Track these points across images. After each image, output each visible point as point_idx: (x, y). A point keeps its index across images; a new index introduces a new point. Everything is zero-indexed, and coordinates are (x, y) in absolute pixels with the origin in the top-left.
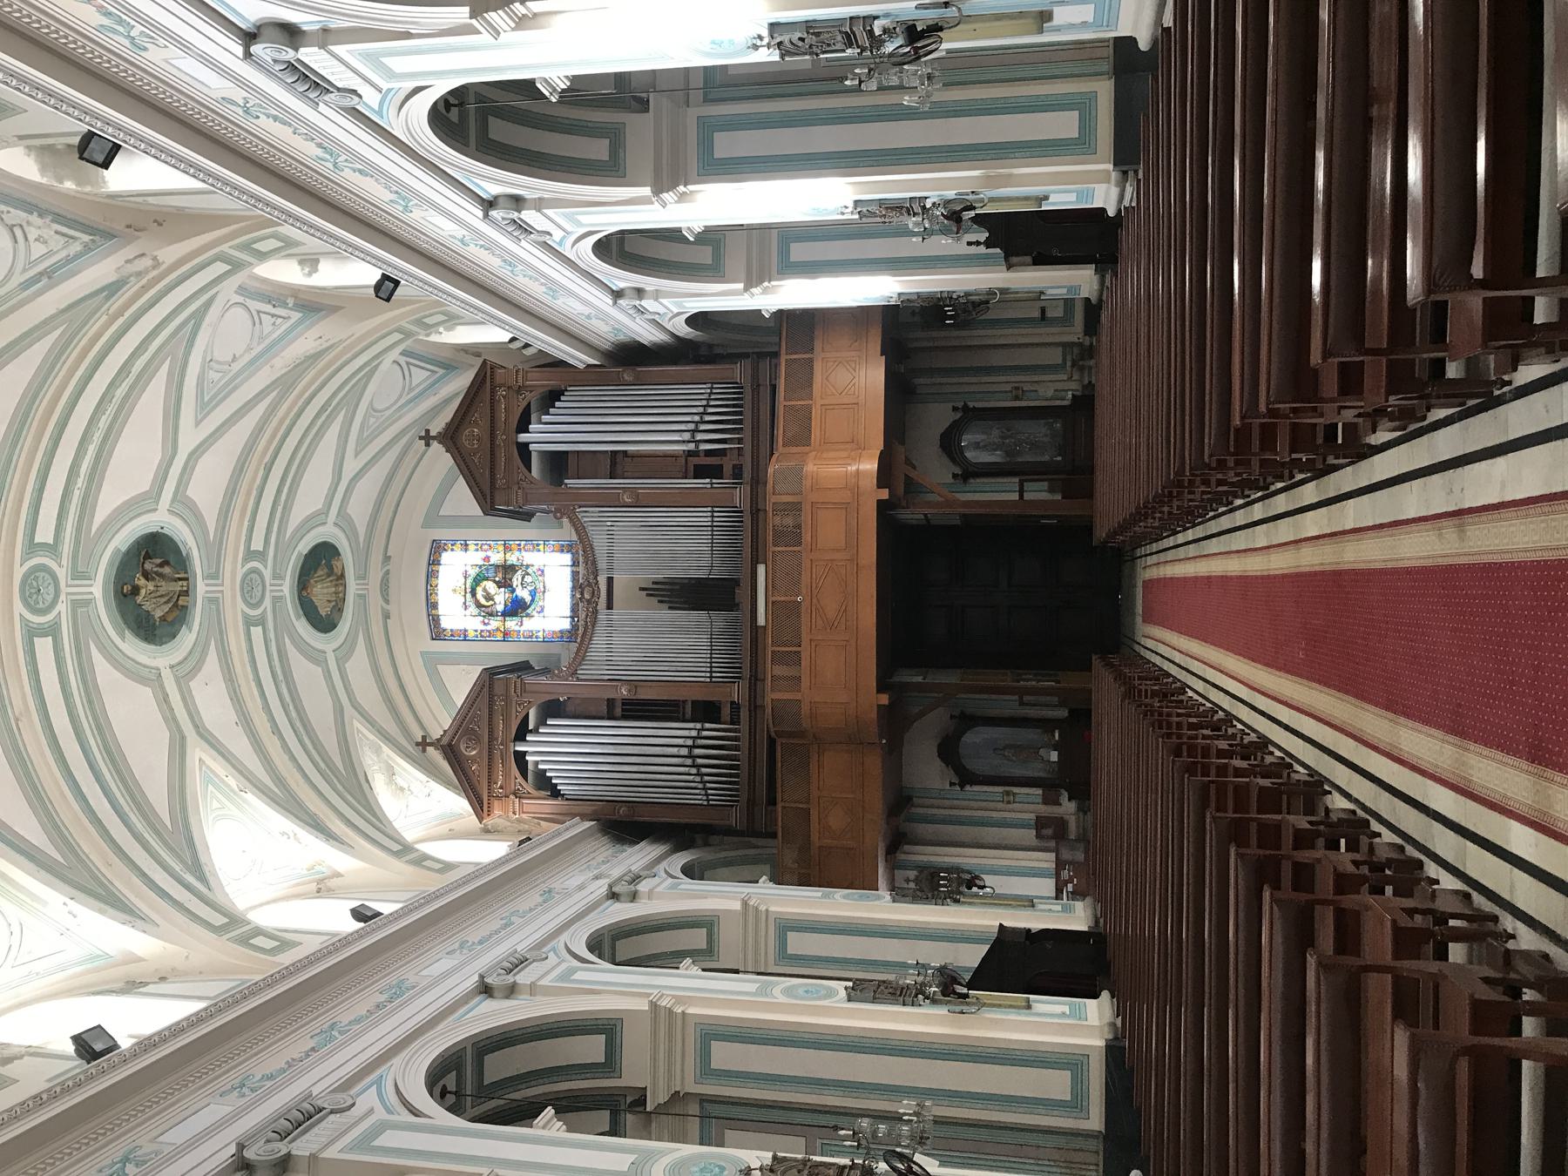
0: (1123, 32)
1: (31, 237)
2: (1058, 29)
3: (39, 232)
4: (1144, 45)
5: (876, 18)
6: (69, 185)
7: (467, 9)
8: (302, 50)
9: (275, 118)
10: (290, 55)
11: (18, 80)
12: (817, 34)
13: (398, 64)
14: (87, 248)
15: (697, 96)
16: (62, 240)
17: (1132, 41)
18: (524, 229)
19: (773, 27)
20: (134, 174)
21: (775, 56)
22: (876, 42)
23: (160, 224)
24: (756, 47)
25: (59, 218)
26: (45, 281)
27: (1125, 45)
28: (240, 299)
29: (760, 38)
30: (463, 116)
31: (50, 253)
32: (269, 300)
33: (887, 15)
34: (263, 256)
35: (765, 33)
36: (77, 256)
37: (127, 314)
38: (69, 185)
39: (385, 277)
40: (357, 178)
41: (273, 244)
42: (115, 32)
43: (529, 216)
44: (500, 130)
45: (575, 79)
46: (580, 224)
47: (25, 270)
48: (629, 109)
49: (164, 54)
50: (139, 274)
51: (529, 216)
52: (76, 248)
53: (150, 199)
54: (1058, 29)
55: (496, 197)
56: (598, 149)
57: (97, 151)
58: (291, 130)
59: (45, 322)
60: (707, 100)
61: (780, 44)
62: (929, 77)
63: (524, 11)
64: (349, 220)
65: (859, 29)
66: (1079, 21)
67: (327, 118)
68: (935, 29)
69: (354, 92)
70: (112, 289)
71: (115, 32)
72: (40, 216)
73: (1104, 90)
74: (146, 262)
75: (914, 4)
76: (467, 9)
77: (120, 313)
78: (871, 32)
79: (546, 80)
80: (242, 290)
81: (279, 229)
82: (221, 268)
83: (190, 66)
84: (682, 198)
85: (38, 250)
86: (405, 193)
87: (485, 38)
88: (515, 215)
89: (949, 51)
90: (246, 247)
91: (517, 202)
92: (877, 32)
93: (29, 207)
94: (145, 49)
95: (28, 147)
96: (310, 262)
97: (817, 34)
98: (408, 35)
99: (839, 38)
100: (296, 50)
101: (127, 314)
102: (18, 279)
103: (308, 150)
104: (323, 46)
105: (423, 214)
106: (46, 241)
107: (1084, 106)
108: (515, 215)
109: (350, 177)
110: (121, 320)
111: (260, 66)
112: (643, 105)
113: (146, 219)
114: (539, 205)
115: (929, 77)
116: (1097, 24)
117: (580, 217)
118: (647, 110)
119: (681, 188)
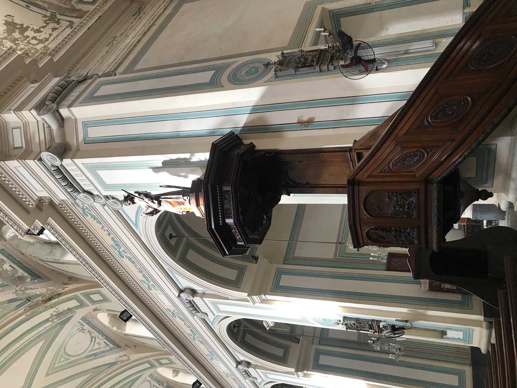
0: (475, 344)
1: (96, 342)
2: (449, 339)
3: (99, 341)
4: (483, 351)
5: (381, 321)
6: (115, 328)
7: (247, 294)
8: (195, 298)
9: (181, 318)
10: (191, 298)
11: (82, 259)
12: (360, 323)
13: (222, 307)
14: (111, 349)
15: (317, 340)
16: (105, 345)
17: (478, 350)
18: (248, 375)
19: (345, 318)
20: (136, 329)
21: (344, 329)
22: (380, 330)
23: (135, 347)
24: (338, 324)
25: (107, 338)
26: (94, 356)
27: (475, 350)
28: (150, 379)
29: (340, 321)
30: (238, 331)
31: (99, 348)
32: (158, 382)
33: (385, 321)
34: (161, 365)
35: (342, 319)
36: (107, 351)
37: (112, 374)
38: (115, 328)
39: (197, 381)
40: (199, 344)
41: (166, 361)
42: (145, 282)
43: (251, 370)
44: (249, 338)
45: (276, 324)
46: (267, 377)
47: (89, 352)
48: (293, 341)
49: (156, 292)
50: (122, 361)
51: (251, 370)
52: (108, 348)
53: (136, 338)
54: (449, 339)
55: (242, 361)
56: (280, 352)
57: (125, 317)
58: (184, 323)
59: (86, 371)
60: (320, 344)
61: (346, 324)
62: (399, 349)
63: (264, 298)
64: (187, 353)
65: (374, 324)
66: (457, 337)
67: (196, 321)
68: (402, 328)
69: (206, 314)
70: (112, 364)
71: (145, 282)
72: (102, 336)
73: (468, 371)
74: (125, 358)
75: (395, 319)
76: (247, 294)
77: (110, 373)
78: (379, 326)
79: (266, 322)
80: (151, 376)
81: (170, 357)
82: (147, 365)
83: (162, 297)
84: (305, 375)
85: (97, 346)
86: (212, 352)
87: (296, 376)
88: (246, 369)
89: (408, 341)
90: (158, 360)
91: (248, 364)
92: (381, 327)
93: (100, 332)
94: (151, 289)
95: (109, 314)
96: (176, 372)
97: (360, 323)
98: (227, 299)
99: (367, 326)
100: (193, 297)
101: (112, 374)
102: (87, 354)
103: (187, 331)
104: (201, 297)
105: (217, 362)
106: (101, 343)
107: (461, 375)
108: (246, 369)
109: (126, 262)
110: (110, 376)
111: (239, 370)
112: (298, 341)
113: (134, 344)
114: (256, 367)
115: (399, 349)
116: (464, 340)
117: (268, 375)
118: (299, 343)
119: (305, 372)
